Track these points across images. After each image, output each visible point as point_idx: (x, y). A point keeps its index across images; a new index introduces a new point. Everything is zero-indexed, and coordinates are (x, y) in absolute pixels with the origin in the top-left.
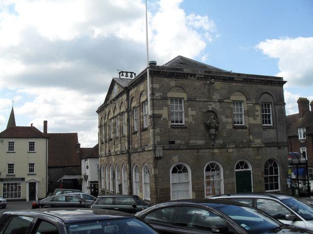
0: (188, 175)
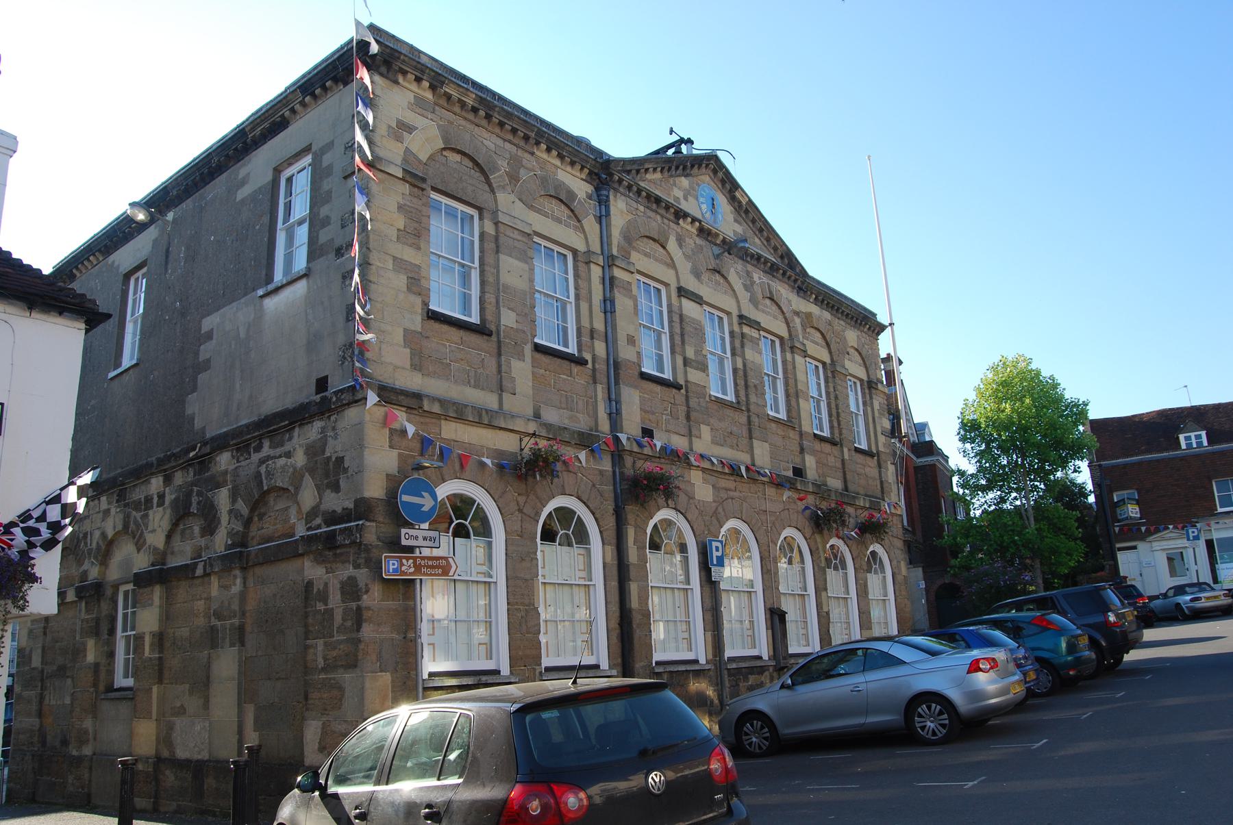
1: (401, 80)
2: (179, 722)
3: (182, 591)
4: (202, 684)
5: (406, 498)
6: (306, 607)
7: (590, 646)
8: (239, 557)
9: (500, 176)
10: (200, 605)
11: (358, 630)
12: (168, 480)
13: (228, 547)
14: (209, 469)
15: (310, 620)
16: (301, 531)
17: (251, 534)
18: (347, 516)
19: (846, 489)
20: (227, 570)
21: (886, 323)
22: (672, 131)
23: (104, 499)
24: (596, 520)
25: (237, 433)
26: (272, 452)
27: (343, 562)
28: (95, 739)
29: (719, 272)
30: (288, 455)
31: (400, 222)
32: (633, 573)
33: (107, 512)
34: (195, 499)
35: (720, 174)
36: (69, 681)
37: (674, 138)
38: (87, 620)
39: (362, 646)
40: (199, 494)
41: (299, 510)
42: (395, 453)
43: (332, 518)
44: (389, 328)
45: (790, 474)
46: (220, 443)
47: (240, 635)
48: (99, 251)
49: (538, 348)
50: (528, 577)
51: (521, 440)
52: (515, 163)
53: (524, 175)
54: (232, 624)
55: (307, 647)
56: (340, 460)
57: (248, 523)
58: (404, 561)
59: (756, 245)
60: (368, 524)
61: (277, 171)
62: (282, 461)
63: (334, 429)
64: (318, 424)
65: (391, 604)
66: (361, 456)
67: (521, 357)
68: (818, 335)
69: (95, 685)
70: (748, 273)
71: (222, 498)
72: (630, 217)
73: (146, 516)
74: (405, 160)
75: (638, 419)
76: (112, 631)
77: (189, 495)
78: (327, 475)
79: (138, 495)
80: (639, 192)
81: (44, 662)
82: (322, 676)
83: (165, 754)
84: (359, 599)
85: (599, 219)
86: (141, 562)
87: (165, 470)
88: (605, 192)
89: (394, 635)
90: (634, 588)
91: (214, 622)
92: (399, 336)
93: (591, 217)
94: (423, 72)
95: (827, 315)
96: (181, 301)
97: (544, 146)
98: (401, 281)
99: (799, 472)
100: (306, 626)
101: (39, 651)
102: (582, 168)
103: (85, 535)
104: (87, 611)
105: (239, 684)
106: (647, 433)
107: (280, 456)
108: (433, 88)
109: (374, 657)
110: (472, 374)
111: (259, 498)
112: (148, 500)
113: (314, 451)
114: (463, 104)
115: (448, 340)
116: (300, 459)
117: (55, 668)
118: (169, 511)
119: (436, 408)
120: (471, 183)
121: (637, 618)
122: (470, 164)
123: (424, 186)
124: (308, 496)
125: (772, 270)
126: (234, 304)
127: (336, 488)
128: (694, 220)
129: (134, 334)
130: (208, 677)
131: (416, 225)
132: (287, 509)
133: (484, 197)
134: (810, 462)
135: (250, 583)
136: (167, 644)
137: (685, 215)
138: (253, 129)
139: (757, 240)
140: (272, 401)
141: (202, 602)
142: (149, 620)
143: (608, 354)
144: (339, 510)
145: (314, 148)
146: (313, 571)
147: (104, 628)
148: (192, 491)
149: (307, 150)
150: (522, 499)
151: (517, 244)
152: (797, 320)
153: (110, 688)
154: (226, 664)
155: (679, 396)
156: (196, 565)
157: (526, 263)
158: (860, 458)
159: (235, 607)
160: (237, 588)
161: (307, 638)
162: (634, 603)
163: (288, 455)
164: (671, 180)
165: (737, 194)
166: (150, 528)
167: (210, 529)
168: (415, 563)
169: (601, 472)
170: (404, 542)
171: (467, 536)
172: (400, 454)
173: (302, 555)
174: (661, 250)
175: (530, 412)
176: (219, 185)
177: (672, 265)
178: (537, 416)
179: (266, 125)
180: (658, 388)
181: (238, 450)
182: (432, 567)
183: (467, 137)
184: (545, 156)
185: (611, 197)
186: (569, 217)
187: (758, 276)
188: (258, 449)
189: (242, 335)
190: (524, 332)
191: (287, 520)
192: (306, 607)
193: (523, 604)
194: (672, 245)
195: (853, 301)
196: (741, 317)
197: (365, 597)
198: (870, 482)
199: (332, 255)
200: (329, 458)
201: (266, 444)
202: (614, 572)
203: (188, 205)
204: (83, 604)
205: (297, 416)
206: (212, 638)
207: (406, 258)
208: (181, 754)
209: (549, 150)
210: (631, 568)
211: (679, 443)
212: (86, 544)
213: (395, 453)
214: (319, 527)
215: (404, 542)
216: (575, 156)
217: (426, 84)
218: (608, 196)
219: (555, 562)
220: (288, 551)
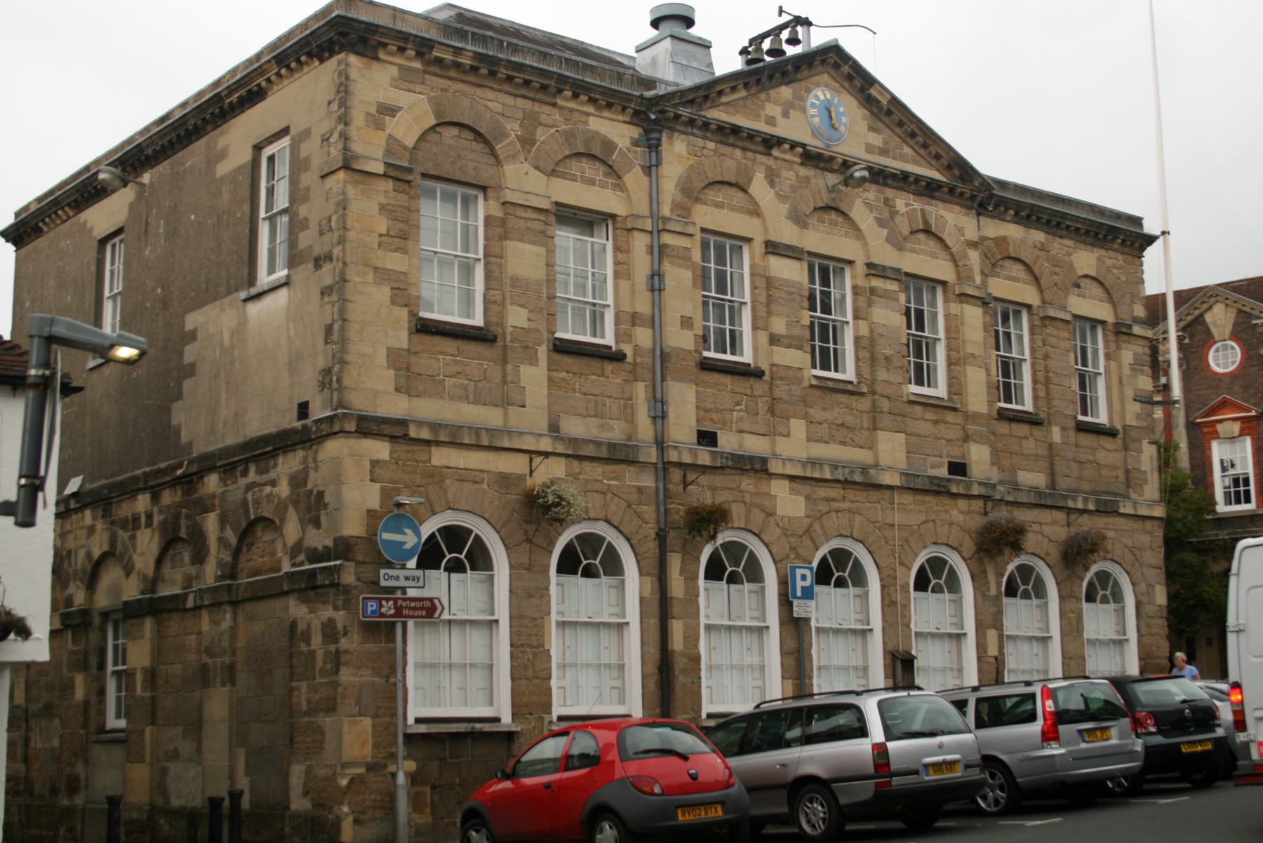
0: (1045, 608)
1: (382, 55)
2: (174, 769)
3: (174, 624)
4: (195, 727)
5: (387, 536)
6: (291, 647)
8: (229, 596)
9: (510, 143)
10: (191, 640)
11: (337, 673)
12: (155, 498)
13: (218, 579)
14: (196, 491)
15: (295, 661)
16: (286, 567)
17: (241, 566)
18: (326, 555)
19: (1053, 485)
20: (216, 605)
21: (1157, 232)
22: (781, 11)
23: (88, 513)
24: (632, 546)
25: (226, 452)
26: (257, 479)
27: (324, 603)
28: (87, 786)
29: (837, 210)
30: (273, 483)
31: (382, 225)
32: (676, 609)
33: (91, 530)
34: (183, 523)
35: (846, 69)
36: (57, 721)
37: (786, 18)
38: (75, 653)
39: (340, 690)
40: (188, 517)
41: (285, 545)
42: (376, 487)
43: (315, 556)
45: (943, 472)
46: (208, 464)
47: (230, 674)
48: (69, 205)
49: (563, 348)
50: (537, 615)
51: (531, 460)
52: (530, 122)
53: (541, 135)
54: (223, 662)
55: (292, 689)
56: (321, 495)
57: (237, 553)
58: (384, 603)
60: (347, 563)
61: (258, 148)
62: (268, 489)
63: (315, 460)
64: (300, 454)
65: (372, 647)
66: (339, 493)
67: (533, 361)
68: (1021, 267)
69: (85, 726)
70: (887, 201)
71: (211, 523)
72: (693, 160)
73: (133, 537)
74: (388, 151)
75: (694, 423)
76: (102, 665)
77: (177, 517)
78: (309, 509)
79: (124, 510)
81: (28, 698)
82: (306, 719)
83: (160, 801)
84: (337, 641)
85: (648, 170)
86: (131, 591)
87: (152, 487)
88: (655, 135)
89: (376, 679)
90: (677, 628)
91: (206, 659)
92: (381, 357)
93: (637, 170)
95: (1038, 236)
96: (163, 288)
97: (568, 93)
98: (385, 292)
99: (958, 468)
100: (291, 667)
101: (22, 686)
102: (624, 109)
103: (69, 552)
104: (74, 642)
105: (230, 727)
106: (707, 438)
107: (265, 484)
108: (420, 55)
109: (353, 702)
110: (471, 388)
111: (251, 528)
112: (136, 519)
113: (298, 481)
114: (458, 66)
115: (441, 353)
116: (284, 489)
117: (41, 705)
118: (157, 534)
119: (425, 434)
120: (471, 161)
121: (679, 663)
122: (470, 136)
123: (410, 178)
124: (292, 529)
125: (929, 189)
126: (218, 303)
127: (317, 524)
128: (794, 145)
129: (114, 317)
130: (200, 718)
131: (402, 226)
132: (273, 541)
133: (486, 174)
134: (979, 457)
135: (241, 619)
136: (160, 682)
137: (780, 141)
138: (230, 94)
139: (907, 150)
140: (257, 424)
141: (193, 637)
142: (139, 654)
143: (654, 344)
144: (320, 547)
145: (293, 132)
146: (297, 609)
147: (94, 661)
148: (180, 513)
149: (285, 131)
152: (974, 256)
153: (102, 730)
154: (217, 704)
155: (760, 387)
156: (185, 596)
157: (542, 245)
159: (225, 644)
160: (227, 622)
161: (292, 680)
162: (677, 643)
163: (273, 483)
164: (763, 96)
165: (873, 92)
166: (138, 551)
167: (199, 557)
168: (395, 604)
169: (640, 490)
170: (383, 583)
171: (463, 570)
172: (382, 488)
173: (286, 593)
174: (741, 195)
175: (543, 426)
176: (194, 154)
177: (755, 212)
178: (554, 428)
179: (243, 92)
180: (727, 379)
181: (225, 471)
182: (415, 609)
183: (466, 103)
184: (572, 105)
185: (664, 139)
186: (606, 175)
187: (904, 203)
188: (245, 473)
189: (227, 341)
190: (538, 331)
191: (273, 554)
192: (291, 647)
193: (531, 646)
194: (759, 187)
195: (1092, 208)
196: (870, 265)
197: (343, 640)
198: (1104, 472)
199: (311, 265)
200: (311, 491)
201: (252, 468)
202: (655, 607)
203: (164, 167)
204: (70, 634)
205: (281, 443)
206: (203, 677)
207: (389, 266)
208: (176, 802)
209: (575, 96)
210: (675, 603)
211: (755, 445)
212: (70, 564)
213: (376, 487)
214: (302, 564)
215: (383, 583)
217: (412, 53)
218: (659, 140)
219: (571, 598)
220: (272, 591)
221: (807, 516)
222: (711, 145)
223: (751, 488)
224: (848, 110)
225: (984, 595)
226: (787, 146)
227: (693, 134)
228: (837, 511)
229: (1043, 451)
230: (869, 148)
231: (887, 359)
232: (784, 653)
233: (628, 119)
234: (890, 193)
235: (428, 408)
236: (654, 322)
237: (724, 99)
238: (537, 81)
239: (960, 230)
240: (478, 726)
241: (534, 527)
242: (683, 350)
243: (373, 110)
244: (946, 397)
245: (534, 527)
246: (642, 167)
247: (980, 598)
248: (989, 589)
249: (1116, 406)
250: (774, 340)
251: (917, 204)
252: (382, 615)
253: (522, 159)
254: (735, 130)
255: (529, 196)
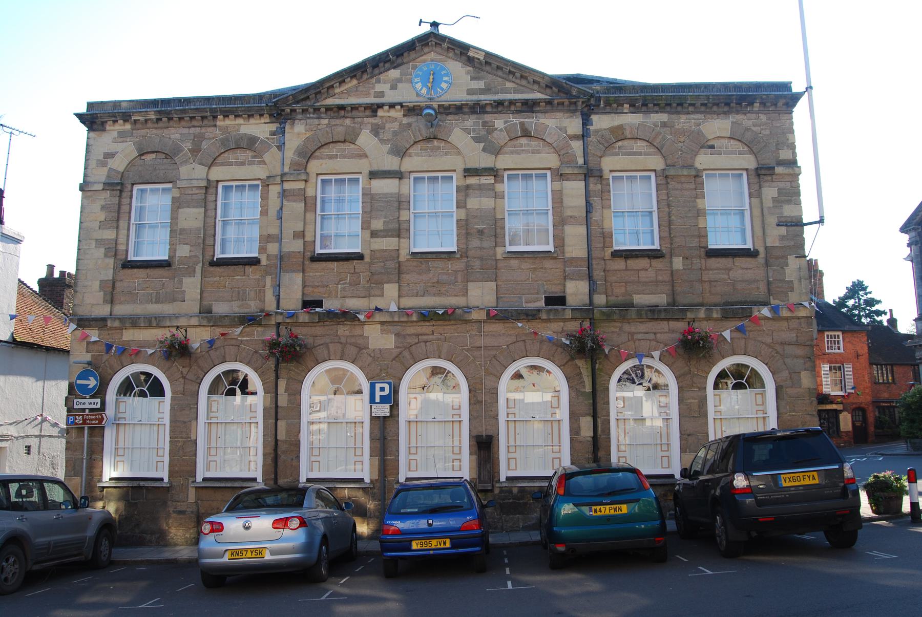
7: (53, 466)
44: (90, 283)
50: (186, 420)
59: (513, 93)
68: (645, 144)
80: (317, 110)
92: (96, 285)
94: (115, 117)
119: (117, 324)
125: (529, 106)
137: (380, 106)
139: (509, 85)
150: (185, 371)
151: (195, 197)
158: (620, 264)
164: (374, 80)
165: (471, 54)
207: (105, 237)
211: (352, 304)
216: (249, 111)
217: (121, 122)
221: (396, 347)
222: (326, 121)
223: (347, 333)
224: (456, 69)
225: (578, 391)
226: (386, 108)
227: (309, 118)
228: (426, 342)
229: (667, 277)
230: (470, 92)
231: (481, 232)
232: (372, 439)
233: (268, 121)
234: (488, 118)
235: (122, 309)
236: (278, 238)
237: (337, 91)
238: (198, 115)
239: (563, 129)
240: (142, 483)
241: (187, 369)
242: (293, 252)
243: (101, 157)
244: (553, 250)
245: (187, 369)
246: (277, 147)
247: (573, 395)
248: (584, 387)
249: (759, 232)
250: (374, 234)
251: (515, 120)
252: (76, 424)
253: (191, 161)
254: (341, 108)
255: (194, 181)
